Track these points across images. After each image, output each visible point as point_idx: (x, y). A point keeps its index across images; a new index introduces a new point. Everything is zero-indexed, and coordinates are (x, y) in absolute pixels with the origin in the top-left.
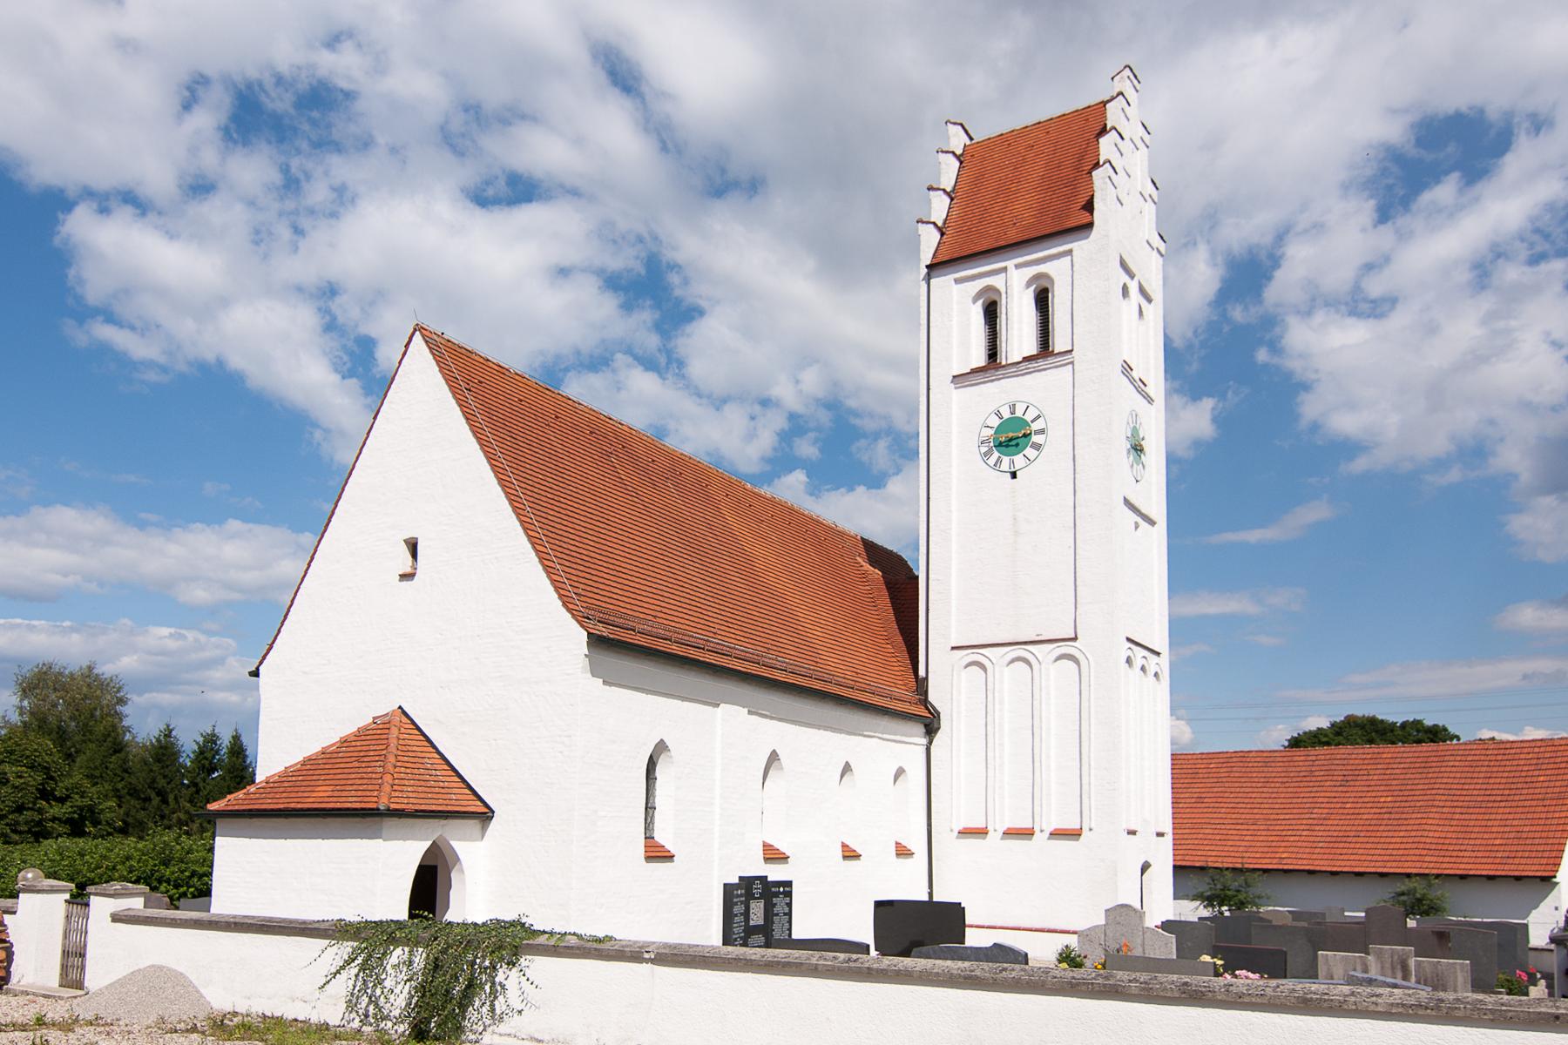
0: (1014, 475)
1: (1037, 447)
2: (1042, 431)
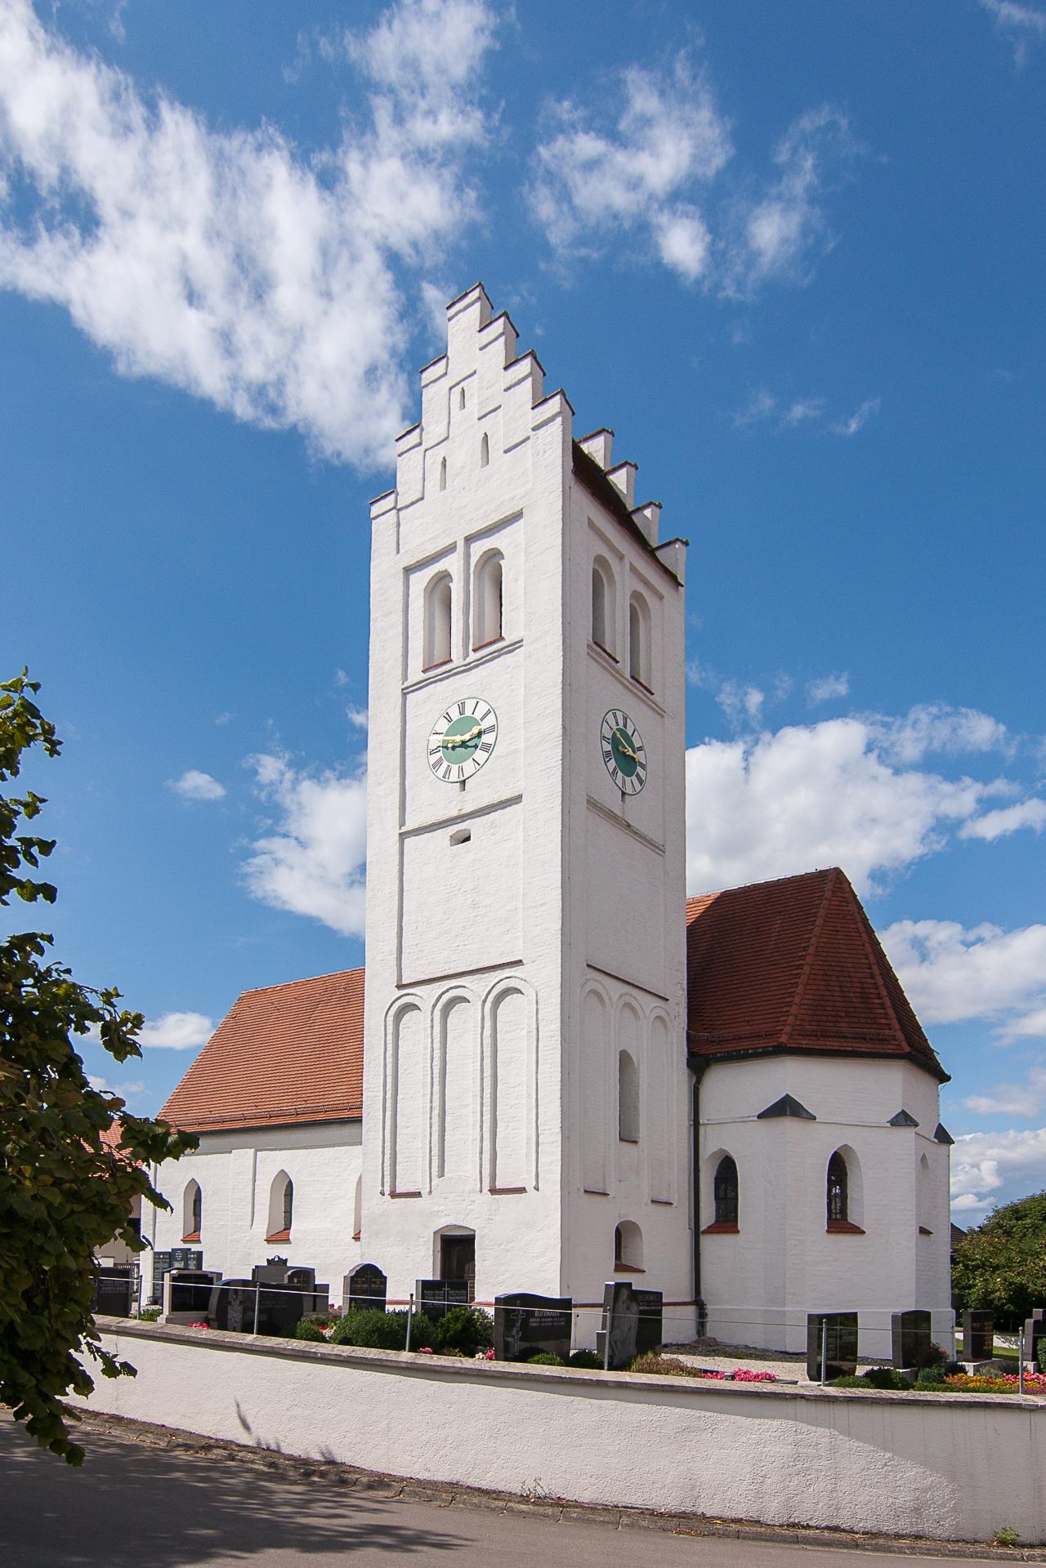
0: (463, 782)
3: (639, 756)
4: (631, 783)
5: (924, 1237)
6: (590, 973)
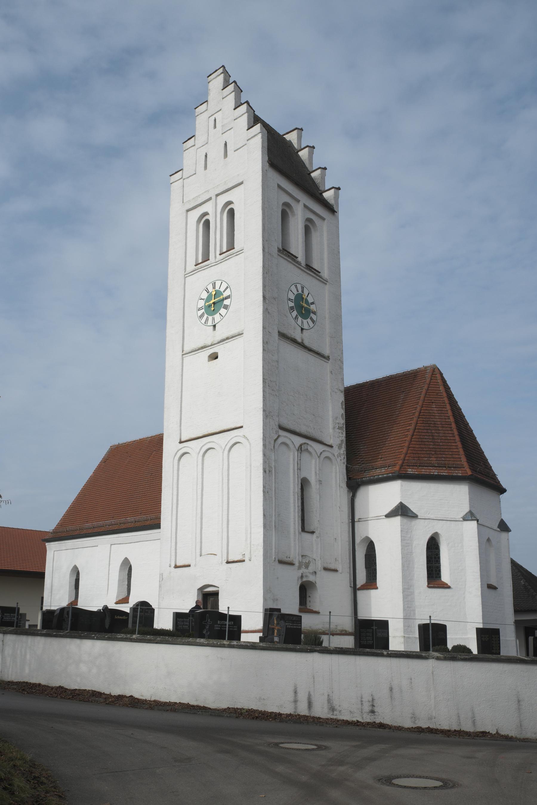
0: (214, 326)
3: (312, 307)
4: (306, 323)
5: (492, 591)
6: (283, 431)
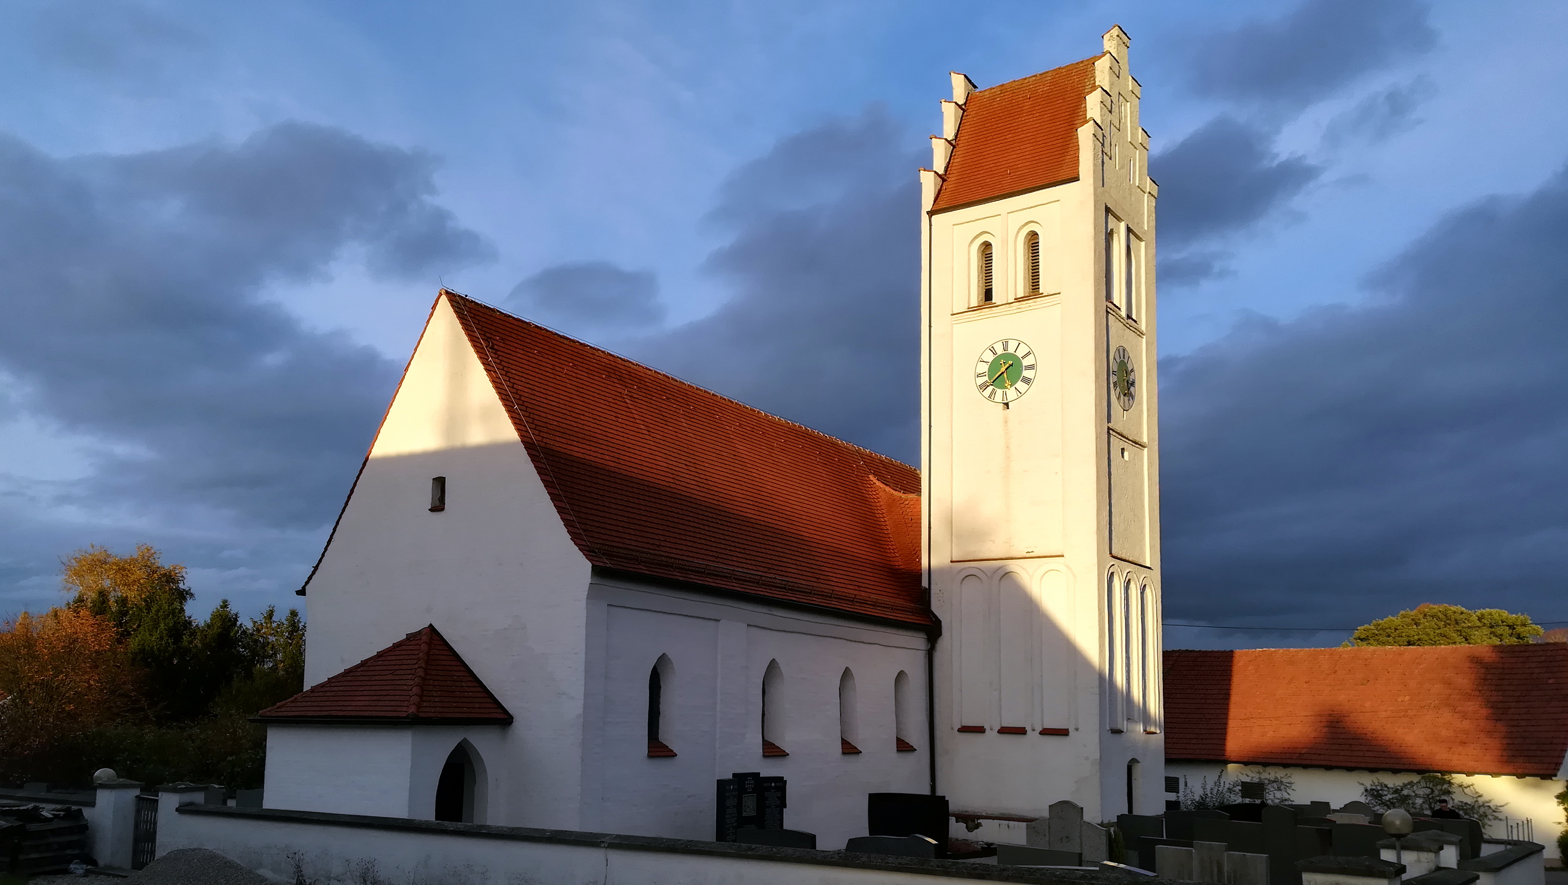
0: (1007, 405)
1: (1027, 381)
2: (1031, 367)
